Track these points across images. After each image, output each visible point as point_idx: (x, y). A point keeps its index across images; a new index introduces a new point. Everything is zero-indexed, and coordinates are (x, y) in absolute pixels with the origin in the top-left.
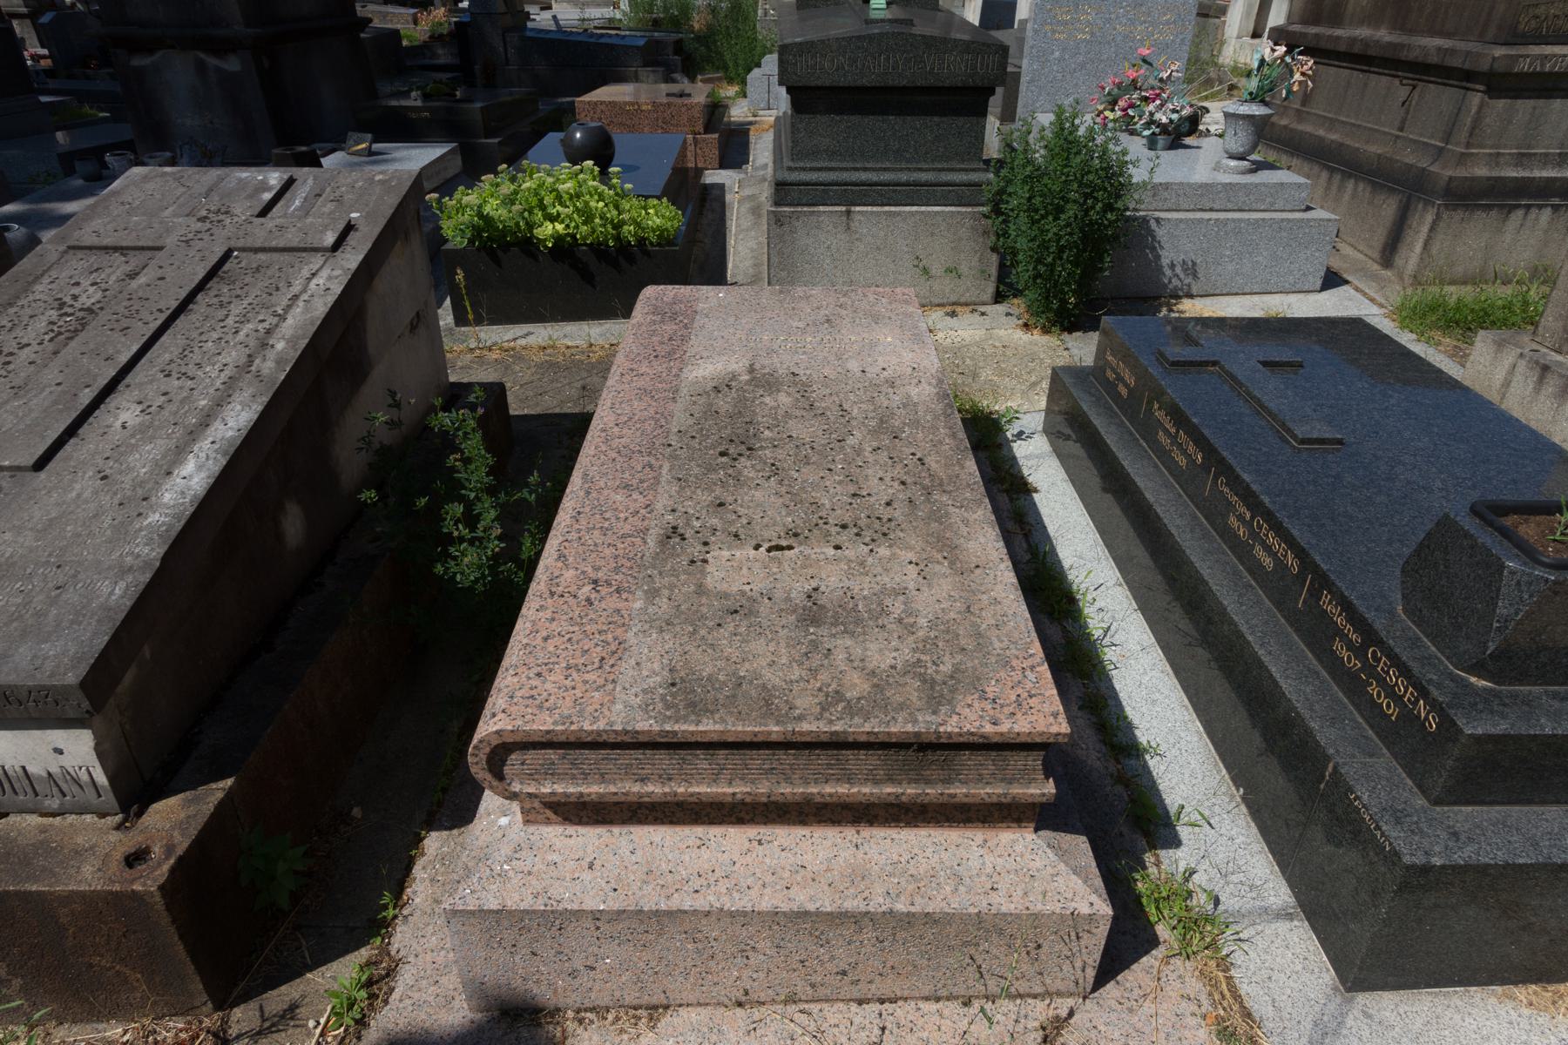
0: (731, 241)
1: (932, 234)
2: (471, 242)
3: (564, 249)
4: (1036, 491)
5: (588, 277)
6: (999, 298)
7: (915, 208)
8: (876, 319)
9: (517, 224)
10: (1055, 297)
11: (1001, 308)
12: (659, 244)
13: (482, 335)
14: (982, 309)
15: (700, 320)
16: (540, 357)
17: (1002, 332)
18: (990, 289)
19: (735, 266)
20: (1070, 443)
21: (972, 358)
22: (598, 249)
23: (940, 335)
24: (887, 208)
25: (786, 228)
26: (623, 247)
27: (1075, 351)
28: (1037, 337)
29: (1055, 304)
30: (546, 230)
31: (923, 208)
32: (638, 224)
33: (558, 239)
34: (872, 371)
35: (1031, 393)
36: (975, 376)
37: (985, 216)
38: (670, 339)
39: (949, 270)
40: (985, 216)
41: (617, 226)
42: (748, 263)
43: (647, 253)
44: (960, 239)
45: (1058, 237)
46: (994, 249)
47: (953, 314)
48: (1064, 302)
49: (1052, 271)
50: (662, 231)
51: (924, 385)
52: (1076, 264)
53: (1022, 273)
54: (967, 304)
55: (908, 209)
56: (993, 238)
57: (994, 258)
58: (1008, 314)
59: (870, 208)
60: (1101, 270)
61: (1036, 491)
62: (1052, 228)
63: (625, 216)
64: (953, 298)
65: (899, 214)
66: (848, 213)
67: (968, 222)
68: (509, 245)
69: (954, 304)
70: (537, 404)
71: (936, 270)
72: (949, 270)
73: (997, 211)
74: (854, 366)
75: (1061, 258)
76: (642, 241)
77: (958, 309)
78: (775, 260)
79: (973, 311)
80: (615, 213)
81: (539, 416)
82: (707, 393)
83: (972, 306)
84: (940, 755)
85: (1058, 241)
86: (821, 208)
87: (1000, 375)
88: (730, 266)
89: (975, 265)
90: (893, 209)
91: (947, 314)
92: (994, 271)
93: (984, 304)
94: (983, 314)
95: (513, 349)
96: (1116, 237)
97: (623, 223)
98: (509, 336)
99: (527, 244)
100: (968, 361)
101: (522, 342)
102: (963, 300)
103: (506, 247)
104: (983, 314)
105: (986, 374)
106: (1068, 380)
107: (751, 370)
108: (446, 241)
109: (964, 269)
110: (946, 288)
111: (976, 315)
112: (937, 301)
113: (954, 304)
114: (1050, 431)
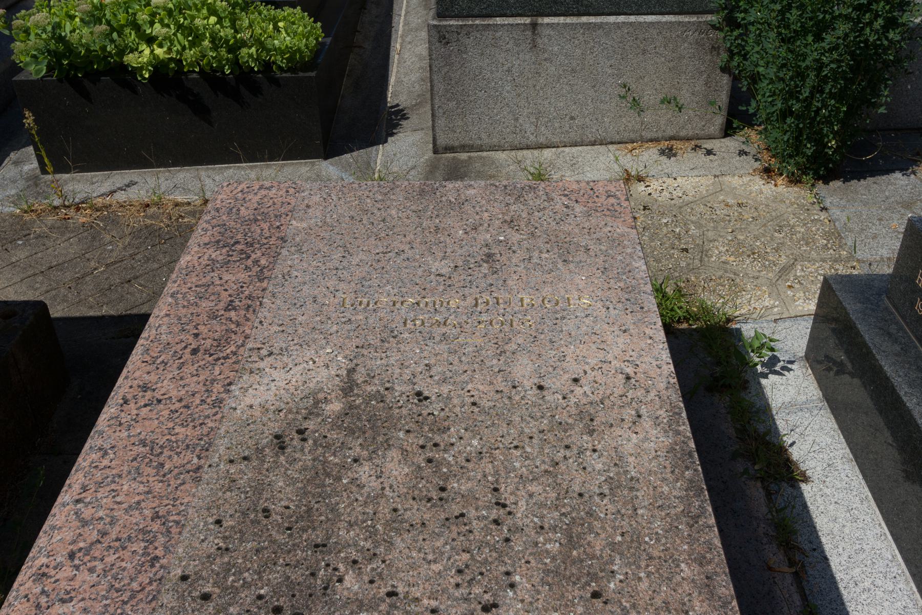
0: (396, 45)
1: (644, 52)
2: (50, 69)
3: (166, 76)
4: (806, 480)
5: (201, 110)
6: (728, 131)
7: (621, 19)
8: (565, 251)
9: (103, 48)
10: (809, 140)
11: (732, 144)
12: (290, 70)
13: (69, 188)
14: (708, 145)
15: (288, 259)
16: (138, 220)
17: (735, 181)
18: (719, 120)
19: (399, 82)
20: (846, 378)
21: (699, 226)
22: (211, 77)
23: (655, 185)
24: (584, 19)
25: (453, 47)
26: (243, 73)
27: (836, 212)
28: (781, 189)
29: (809, 149)
30: (142, 57)
31: (632, 18)
32: (261, 44)
33: (159, 67)
34: (557, 383)
35: (782, 286)
36: (704, 253)
37: (713, 27)
38: (230, 307)
39: (666, 101)
40: (713, 27)
41: (234, 49)
42: (414, 77)
43: (275, 82)
44: (681, 57)
45: (820, 66)
46: (725, 69)
47: (669, 153)
48: (821, 144)
49: (808, 107)
50: (293, 52)
51: (646, 423)
52: (840, 97)
53: (765, 101)
54: (688, 139)
55: (612, 19)
56: (725, 56)
57: (725, 80)
58: (742, 153)
59: (562, 20)
60: (876, 105)
61: (806, 480)
62: (812, 50)
63: (245, 35)
64: (670, 132)
65: (600, 26)
66: (534, 26)
67: (692, 36)
68: (98, 73)
69: (671, 138)
70: (121, 299)
71: (650, 97)
72: (666, 101)
73: (731, 22)
74: (524, 370)
75: (822, 92)
76: (267, 66)
77: (677, 145)
78: (440, 87)
79: (696, 148)
80: (230, 31)
81: (121, 317)
82: (259, 451)
83: (695, 141)
84: (626, 136)
85: (819, 69)
86: (499, 21)
87: (736, 254)
88: (392, 80)
89: (702, 90)
90: (592, 19)
91: (662, 152)
92: (723, 98)
93: (710, 138)
94: (709, 152)
95: (107, 207)
96: (898, 61)
97: (243, 44)
98: (106, 187)
99: (123, 75)
100: (693, 231)
101: (121, 197)
102: (683, 133)
103: (93, 76)
104: (709, 152)
105: (719, 251)
106: (852, 308)
107: (349, 387)
108: (21, 70)
109: (685, 97)
110: (662, 120)
111: (700, 152)
112: (648, 135)
113: (671, 138)
114: (816, 357)
